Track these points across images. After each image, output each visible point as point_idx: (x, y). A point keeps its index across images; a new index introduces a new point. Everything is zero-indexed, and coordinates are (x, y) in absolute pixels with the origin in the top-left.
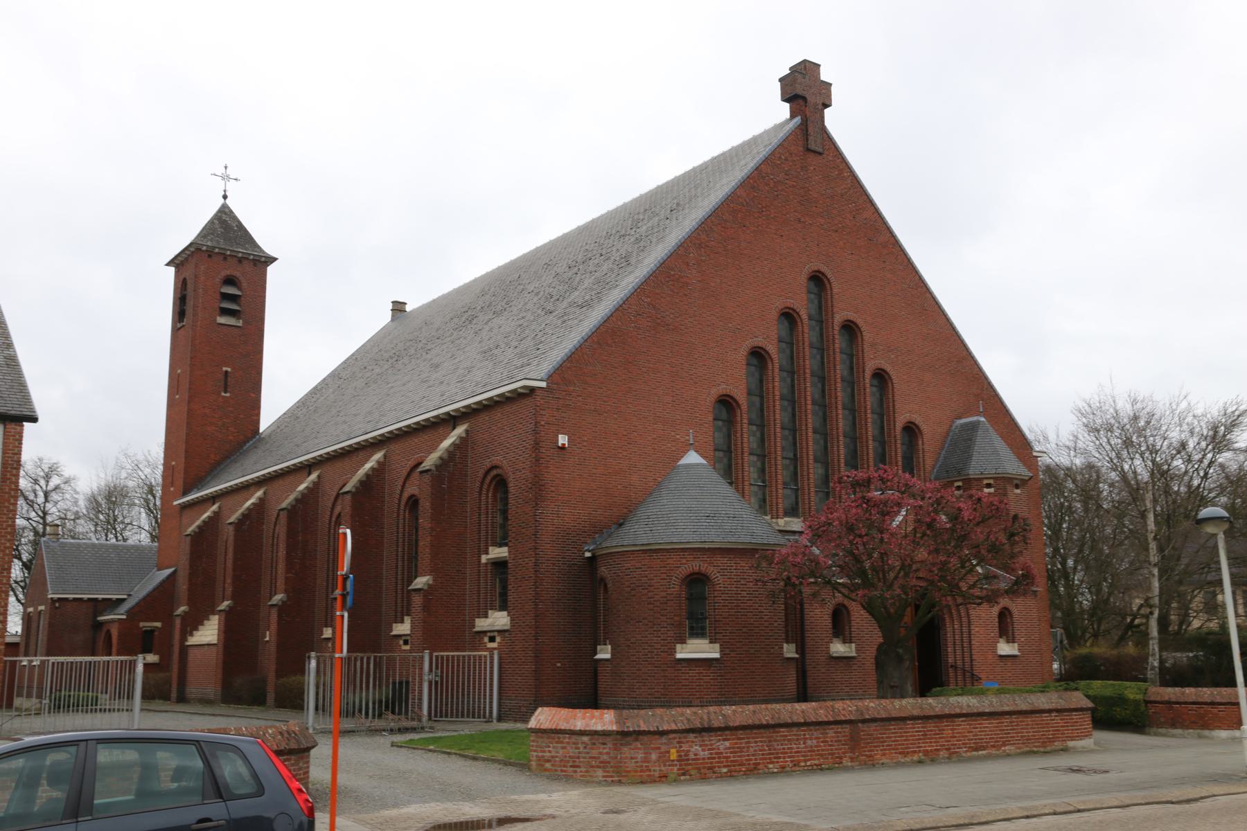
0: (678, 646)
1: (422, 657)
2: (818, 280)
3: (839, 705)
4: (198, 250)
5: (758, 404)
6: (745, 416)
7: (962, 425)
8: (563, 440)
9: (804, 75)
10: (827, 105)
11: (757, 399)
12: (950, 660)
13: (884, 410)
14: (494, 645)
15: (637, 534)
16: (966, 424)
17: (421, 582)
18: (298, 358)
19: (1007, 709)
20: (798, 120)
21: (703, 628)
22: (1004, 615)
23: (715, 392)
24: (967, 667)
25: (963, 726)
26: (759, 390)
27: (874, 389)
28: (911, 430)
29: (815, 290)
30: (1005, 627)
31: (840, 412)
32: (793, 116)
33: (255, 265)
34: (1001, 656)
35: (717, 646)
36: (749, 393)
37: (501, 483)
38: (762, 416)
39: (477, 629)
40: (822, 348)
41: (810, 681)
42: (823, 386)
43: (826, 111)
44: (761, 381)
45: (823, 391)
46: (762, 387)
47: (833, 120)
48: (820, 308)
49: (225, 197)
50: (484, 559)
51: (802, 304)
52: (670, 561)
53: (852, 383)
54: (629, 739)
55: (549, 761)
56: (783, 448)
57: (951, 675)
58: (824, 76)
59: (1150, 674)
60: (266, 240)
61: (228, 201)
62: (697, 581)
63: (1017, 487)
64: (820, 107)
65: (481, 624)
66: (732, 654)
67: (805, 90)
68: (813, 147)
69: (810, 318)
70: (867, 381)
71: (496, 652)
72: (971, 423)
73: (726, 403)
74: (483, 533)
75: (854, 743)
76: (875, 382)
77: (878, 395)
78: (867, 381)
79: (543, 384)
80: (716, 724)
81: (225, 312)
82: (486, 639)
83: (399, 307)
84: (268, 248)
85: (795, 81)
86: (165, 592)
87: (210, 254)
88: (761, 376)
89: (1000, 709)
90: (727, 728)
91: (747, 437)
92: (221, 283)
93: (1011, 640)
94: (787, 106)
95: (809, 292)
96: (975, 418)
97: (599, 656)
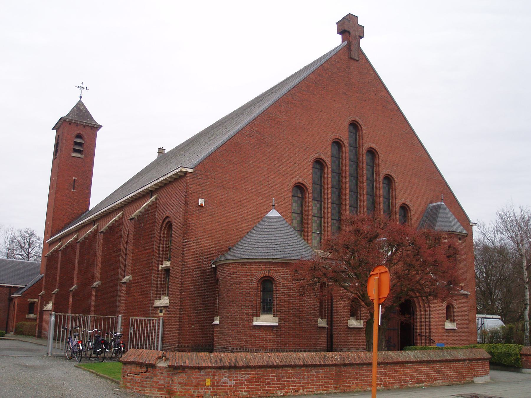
0: (255, 318)
1: (117, 319)
2: (354, 126)
3: (351, 355)
4: (65, 121)
5: (319, 190)
6: (310, 195)
7: (432, 207)
8: (201, 201)
9: (349, 21)
10: (361, 37)
11: (318, 187)
12: (418, 331)
13: (390, 197)
14: (161, 314)
15: (240, 252)
16: (434, 206)
17: (127, 278)
18: (110, 176)
19: (438, 358)
20: (345, 43)
21: (270, 308)
22: (449, 308)
23: (294, 181)
24: (428, 335)
25: (410, 369)
26: (320, 183)
27: (385, 185)
28: (405, 208)
29: (354, 131)
30: (449, 315)
31: (365, 196)
32: (343, 41)
33: (92, 129)
34: (446, 329)
35: (277, 319)
36: (314, 183)
37: (170, 226)
38: (321, 196)
39: (155, 306)
40: (356, 161)
41: (335, 341)
42: (357, 182)
43: (361, 40)
44: (321, 177)
45: (357, 185)
46: (321, 180)
47: (364, 44)
48: (356, 140)
49: (81, 97)
50: (161, 267)
51: (345, 137)
52: (252, 269)
53: (372, 181)
54: (178, 371)
55: (129, 382)
56: (332, 214)
57: (419, 339)
58: (360, 22)
59: (525, 340)
60: (98, 119)
61: (82, 100)
62: (267, 282)
63: (460, 239)
64: (358, 37)
65: (158, 303)
66: (286, 324)
67: (350, 29)
68: (353, 57)
69: (350, 145)
70: (381, 180)
71: (161, 318)
72: (437, 205)
73: (300, 187)
74: (161, 254)
75: (338, 379)
76: (386, 182)
77: (387, 188)
78: (381, 180)
79: (191, 171)
80: (241, 364)
81: (75, 151)
82: (159, 311)
83: (161, 151)
84: (99, 121)
85: (344, 23)
86: (37, 287)
87: (70, 123)
88: (321, 174)
89: (434, 359)
90: (248, 367)
91: (313, 208)
92: (76, 136)
93: (453, 321)
94: (340, 36)
95: (350, 132)
96: (439, 203)
97: (215, 323)
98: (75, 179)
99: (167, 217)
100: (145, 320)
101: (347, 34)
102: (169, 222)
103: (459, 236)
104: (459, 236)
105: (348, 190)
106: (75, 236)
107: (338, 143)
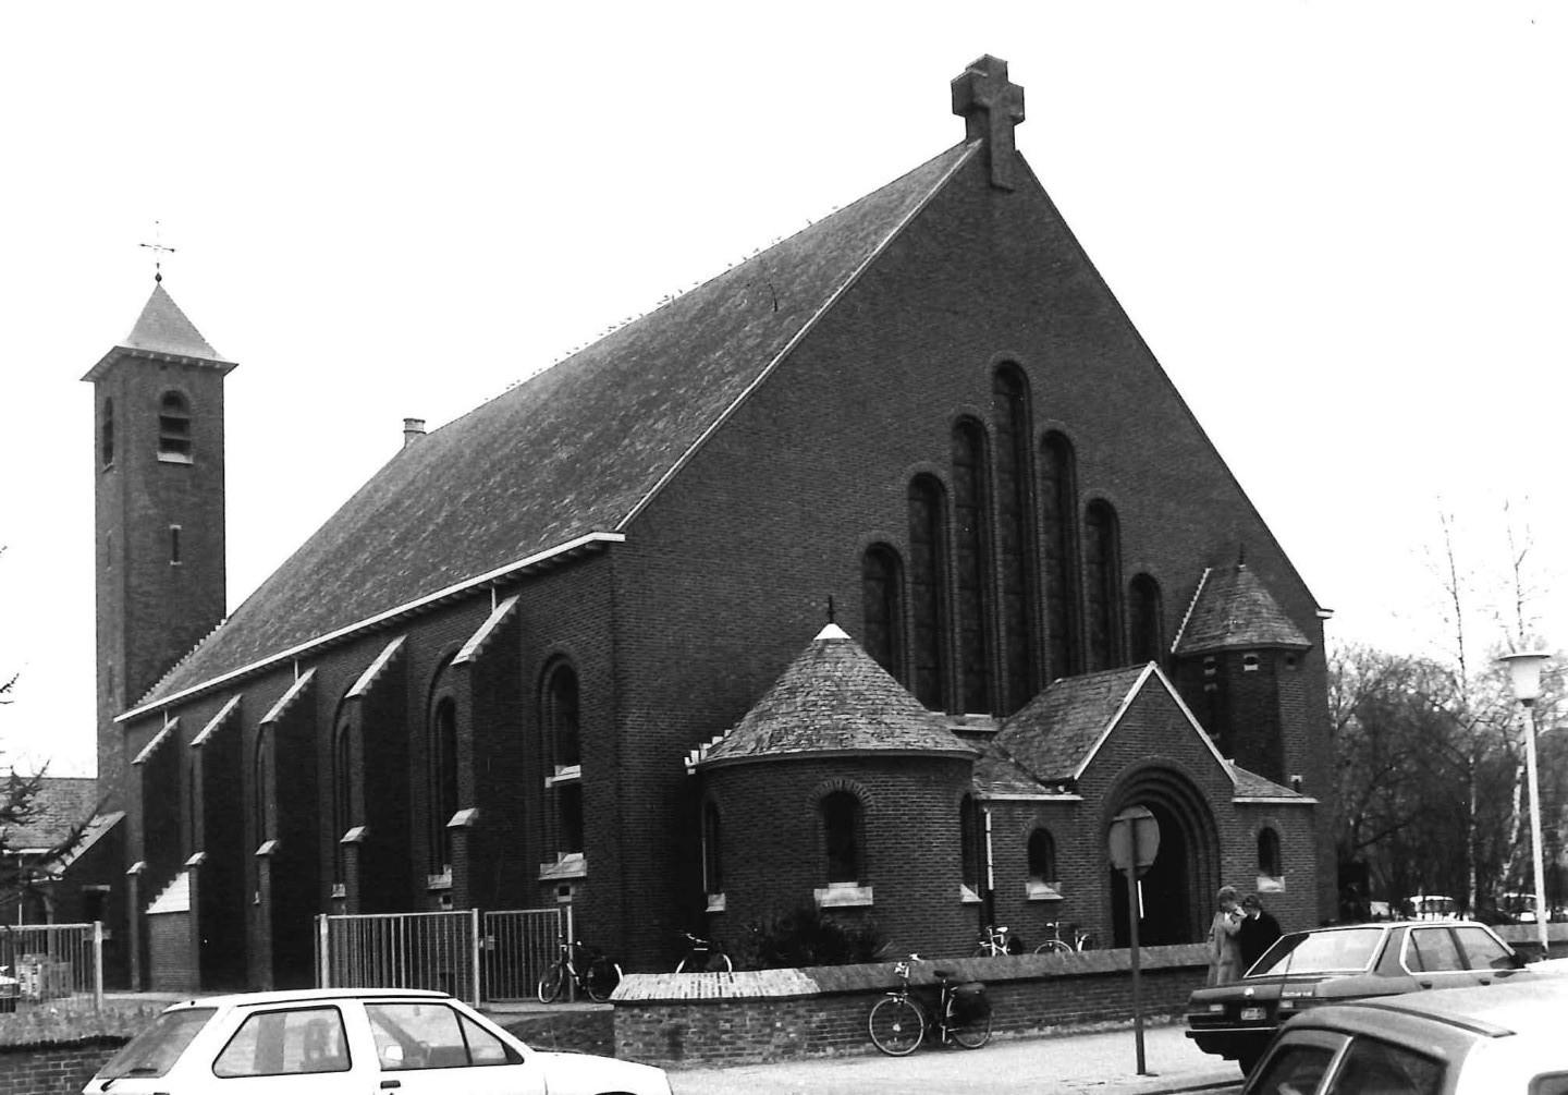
2: (1010, 377)
14: (567, 899)
18: (277, 508)
36: (914, 539)
50: (548, 782)
51: (989, 414)
65: (549, 872)
67: (986, 98)
68: (998, 181)
79: (621, 538)
81: (168, 446)
82: (556, 891)
94: (962, 121)
98: (175, 531)
99: (558, 656)
100: (389, 920)
101: (980, 115)
102: (563, 667)
103: (1288, 654)
104: (1288, 654)
105: (999, 550)
106: (233, 702)
107: (969, 429)
